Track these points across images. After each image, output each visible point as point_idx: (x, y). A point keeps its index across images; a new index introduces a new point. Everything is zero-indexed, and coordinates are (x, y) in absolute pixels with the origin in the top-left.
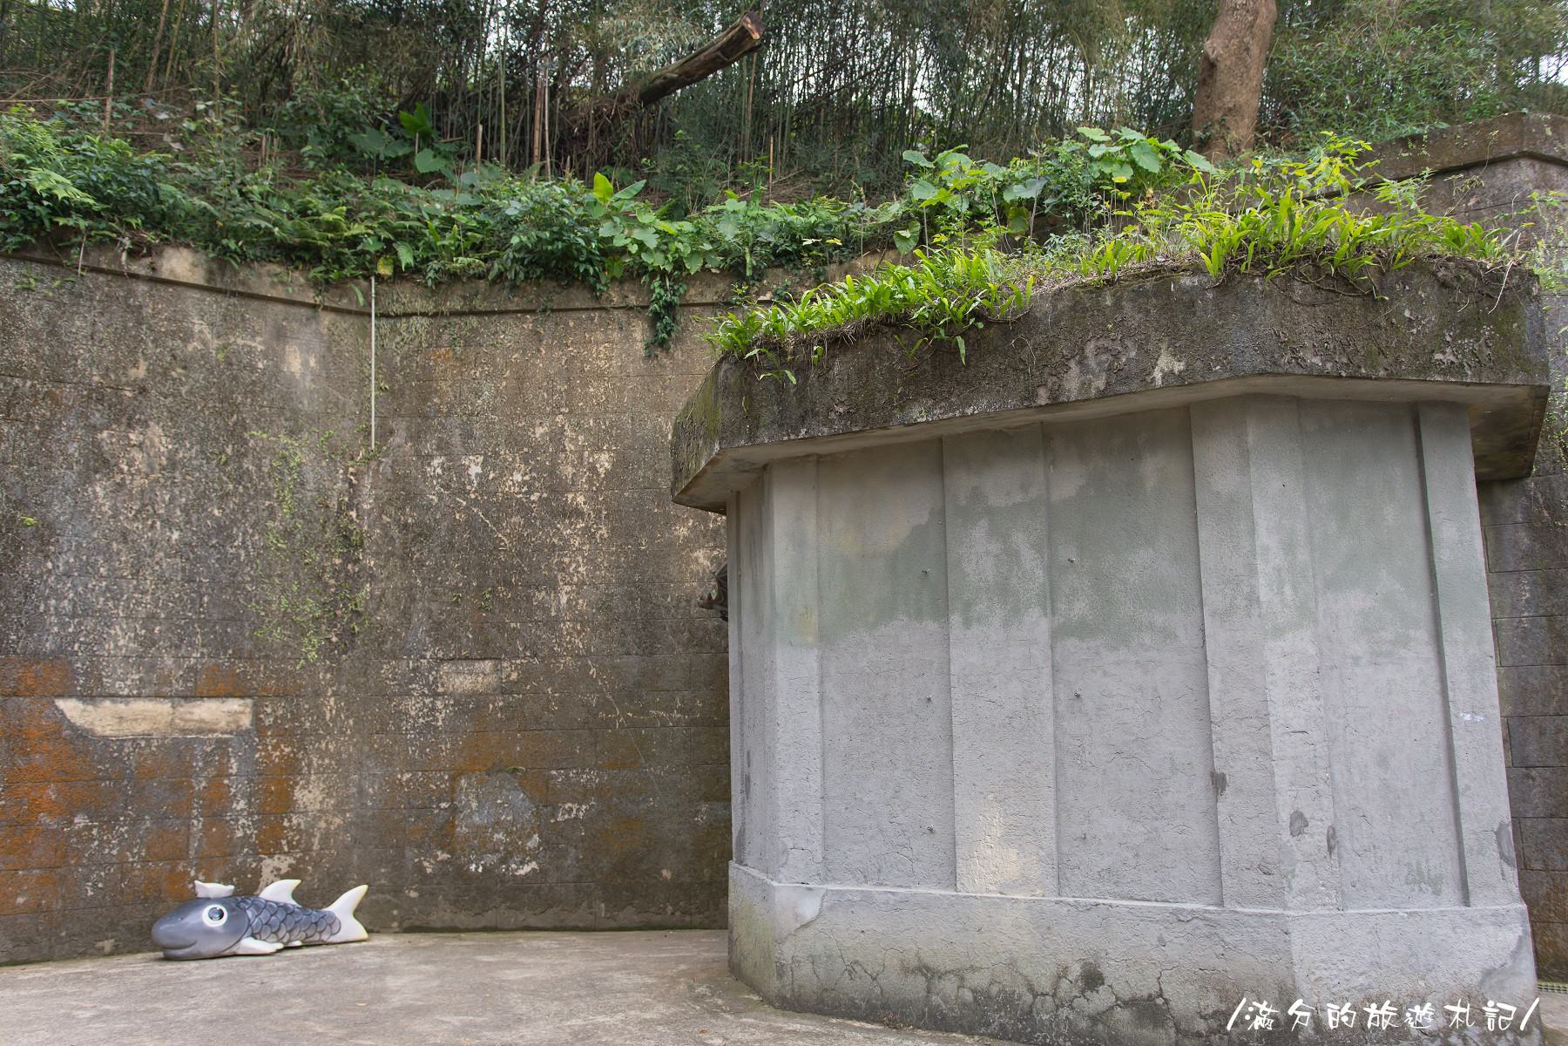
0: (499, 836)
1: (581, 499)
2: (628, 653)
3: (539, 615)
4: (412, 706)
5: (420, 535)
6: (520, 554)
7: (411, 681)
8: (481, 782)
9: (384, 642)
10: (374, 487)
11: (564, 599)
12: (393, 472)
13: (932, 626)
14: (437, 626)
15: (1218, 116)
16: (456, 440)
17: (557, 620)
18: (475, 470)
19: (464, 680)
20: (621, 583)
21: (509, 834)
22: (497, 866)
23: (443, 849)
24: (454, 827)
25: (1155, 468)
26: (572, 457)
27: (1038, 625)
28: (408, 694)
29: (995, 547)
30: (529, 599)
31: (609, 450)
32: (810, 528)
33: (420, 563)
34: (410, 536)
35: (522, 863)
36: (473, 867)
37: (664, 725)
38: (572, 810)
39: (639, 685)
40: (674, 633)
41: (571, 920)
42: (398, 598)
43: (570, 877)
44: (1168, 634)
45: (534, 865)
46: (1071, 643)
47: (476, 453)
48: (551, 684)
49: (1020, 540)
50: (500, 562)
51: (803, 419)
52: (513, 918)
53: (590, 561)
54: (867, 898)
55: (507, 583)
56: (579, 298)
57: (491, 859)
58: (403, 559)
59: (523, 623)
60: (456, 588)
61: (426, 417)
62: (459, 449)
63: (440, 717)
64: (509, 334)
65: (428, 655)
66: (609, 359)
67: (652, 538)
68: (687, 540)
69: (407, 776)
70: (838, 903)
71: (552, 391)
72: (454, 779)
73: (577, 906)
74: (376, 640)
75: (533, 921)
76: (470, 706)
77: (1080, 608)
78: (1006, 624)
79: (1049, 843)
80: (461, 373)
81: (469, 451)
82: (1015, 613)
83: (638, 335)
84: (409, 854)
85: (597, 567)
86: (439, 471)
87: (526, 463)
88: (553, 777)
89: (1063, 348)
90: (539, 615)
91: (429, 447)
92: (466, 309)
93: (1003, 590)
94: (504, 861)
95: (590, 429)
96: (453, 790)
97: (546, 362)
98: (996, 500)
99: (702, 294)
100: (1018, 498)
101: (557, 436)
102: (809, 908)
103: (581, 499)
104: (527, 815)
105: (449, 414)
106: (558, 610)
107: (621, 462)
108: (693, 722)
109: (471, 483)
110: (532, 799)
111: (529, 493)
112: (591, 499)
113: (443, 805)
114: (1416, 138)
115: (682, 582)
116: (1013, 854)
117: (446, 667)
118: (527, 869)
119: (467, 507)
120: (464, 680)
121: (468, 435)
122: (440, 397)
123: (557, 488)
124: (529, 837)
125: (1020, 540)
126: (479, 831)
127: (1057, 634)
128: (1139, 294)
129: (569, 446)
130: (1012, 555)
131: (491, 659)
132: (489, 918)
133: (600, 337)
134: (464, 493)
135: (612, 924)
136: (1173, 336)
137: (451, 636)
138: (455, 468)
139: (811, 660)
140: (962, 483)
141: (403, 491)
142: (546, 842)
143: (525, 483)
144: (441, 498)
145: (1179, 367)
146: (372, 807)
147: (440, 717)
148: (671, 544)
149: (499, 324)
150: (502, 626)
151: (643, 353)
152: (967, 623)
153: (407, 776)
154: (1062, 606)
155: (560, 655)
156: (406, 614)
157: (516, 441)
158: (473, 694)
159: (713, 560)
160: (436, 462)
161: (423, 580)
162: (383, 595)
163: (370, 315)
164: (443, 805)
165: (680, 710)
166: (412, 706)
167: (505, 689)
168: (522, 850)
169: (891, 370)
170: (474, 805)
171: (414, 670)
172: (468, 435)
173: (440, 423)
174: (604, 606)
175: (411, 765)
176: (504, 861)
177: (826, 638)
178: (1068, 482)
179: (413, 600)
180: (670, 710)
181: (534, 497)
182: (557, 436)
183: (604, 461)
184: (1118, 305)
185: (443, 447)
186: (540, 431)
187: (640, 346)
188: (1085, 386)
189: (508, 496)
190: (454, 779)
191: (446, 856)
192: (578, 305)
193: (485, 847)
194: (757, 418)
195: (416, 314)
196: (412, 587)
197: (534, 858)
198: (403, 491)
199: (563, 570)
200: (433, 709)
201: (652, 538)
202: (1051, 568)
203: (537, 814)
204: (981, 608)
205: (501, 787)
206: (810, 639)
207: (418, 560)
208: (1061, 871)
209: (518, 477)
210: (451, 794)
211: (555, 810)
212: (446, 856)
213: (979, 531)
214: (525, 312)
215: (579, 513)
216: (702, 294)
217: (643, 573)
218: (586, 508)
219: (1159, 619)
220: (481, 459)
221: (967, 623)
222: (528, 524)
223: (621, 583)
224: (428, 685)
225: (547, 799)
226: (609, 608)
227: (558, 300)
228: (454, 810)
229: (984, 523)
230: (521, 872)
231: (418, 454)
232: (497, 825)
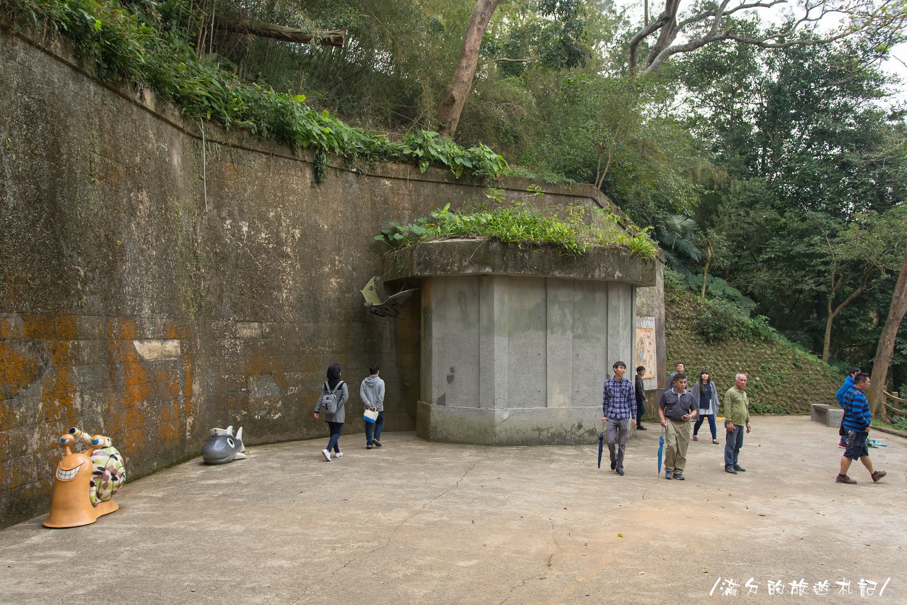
0: (266, 402)
1: (289, 250)
2: (309, 322)
3: (276, 303)
4: (226, 343)
5: (223, 258)
6: (266, 273)
7: (225, 331)
8: (258, 379)
9: (211, 311)
10: (201, 231)
11: (285, 296)
12: (209, 225)
13: (541, 333)
14: (234, 305)
15: (450, 120)
16: (236, 212)
17: (283, 305)
18: (245, 229)
19: (249, 331)
20: (306, 290)
21: (270, 401)
22: (266, 416)
23: (244, 410)
24: (248, 399)
25: (599, 296)
26: (285, 229)
27: (570, 335)
28: (224, 337)
29: (560, 312)
30: (271, 294)
31: (299, 228)
32: (506, 299)
33: (224, 273)
34: (219, 259)
35: (275, 414)
36: (256, 417)
37: (323, 353)
38: (293, 390)
39: (313, 335)
40: (325, 313)
41: (294, 436)
42: (216, 290)
43: (293, 419)
44: (599, 340)
45: (280, 414)
46: (577, 340)
47: (245, 220)
48: (282, 334)
49: (567, 311)
50: (258, 276)
51: (522, 268)
52: (273, 438)
53: (293, 279)
54: (523, 412)
55: (262, 286)
56: (287, 152)
57: (263, 413)
58: (216, 270)
59: (270, 306)
60: (240, 287)
61: (222, 198)
62: (237, 217)
63: (239, 348)
64: (256, 163)
65: (231, 318)
66: (297, 184)
67: (316, 271)
68: (328, 274)
69: (226, 376)
70: (512, 414)
71: (275, 195)
72: (247, 377)
73: (296, 430)
74: (208, 310)
75: (281, 438)
76: (249, 343)
77: (579, 331)
78: (562, 334)
79: (570, 393)
80: (238, 178)
81: (243, 219)
82: (564, 331)
83: (308, 175)
84: (230, 413)
85: (296, 282)
86: (229, 227)
87: (267, 229)
88: (286, 376)
89: (595, 264)
90: (276, 303)
91: (224, 214)
92: (239, 145)
93: (562, 325)
94: (269, 413)
95: (291, 217)
96: (247, 382)
97: (274, 181)
98: (561, 299)
99: (332, 162)
100: (567, 299)
101: (278, 218)
102: (506, 416)
103: (289, 250)
104: (277, 393)
105: (232, 198)
106: (283, 301)
107: (303, 235)
108: (333, 352)
109: (244, 235)
110: (278, 386)
111: (268, 244)
112: (293, 250)
113: (243, 390)
114: (569, 183)
115: (327, 292)
116: (562, 397)
117: (239, 325)
118: (277, 416)
119: (243, 247)
120: (249, 331)
121: (241, 211)
122: (229, 189)
123: (280, 243)
124: (278, 402)
125: (567, 311)
126: (258, 400)
127: (574, 337)
128: (613, 254)
129: (284, 224)
130: (565, 315)
131: (257, 322)
132: (264, 438)
133: (293, 173)
134: (241, 240)
135: (309, 436)
136: (620, 267)
137: (241, 310)
138: (236, 228)
139: (506, 340)
140: (552, 292)
141: (214, 236)
142: (283, 404)
143: (266, 239)
144: (231, 241)
145: (620, 275)
146: (212, 392)
147: (239, 348)
148: (323, 275)
149: (251, 156)
150: (261, 307)
151: (310, 185)
152: (552, 333)
153: (226, 376)
154: (575, 330)
155: (284, 322)
156: (220, 298)
157: (262, 217)
158: (251, 338)
159: (338, 283)
160: (228, 222)
161: (226, 281)
162: (209, 287)
163: (202, 139)
164: (243, 390)
165: (328, 347)
166: (226, 343)
167: (263, 336)
168: (275, 408)
169: (550, 258)
170: (256, 389)
171: (226, 326)
172: (241, 211)
173: (228, 202)
174: (299, 300)
175: (227, 371)
176: (269, 413)
177: (510, 335)
178: (578, 296)
179: (223, 291)
180: (324, 346)
181: (270, 246)
182: (278, 218)
183: (297, 233)
184: (608, 255)
185: (231, 215)
186: (272, 214)
187: (309, 181)
188: (600, 275)
189: (260, 244)
190: (247, 377)
191: (246, 413)
192: (285, 155)
193: (260, 409)
194: (507, 264)
195: (216, 142)
196: (221, 284)
197: (280, 411)
198: (214, 236)
199: (284, 282)
200: (236, 345)
201: (316, 271)
202: (574, 320)
203: (280, 392)
204: (556, 329)
205: (266, 381)
206: (506, 334)
207: (223, 271)
208: (572, 399)
209: (263, 235)
210: (246, 384)
211: (287, 390)
212: (246, 413)
213: (556, 307)
214: (263, 153)
215: (288, 256)
216: (332, 162)
217: (313, 287)
218: (291, 254)
219: (597, 336)
220: (247, 224)
221: (552, 333)
222: (269, 259)
223: (306, 290)
224: (232, 333)
225: (284, 387)
226: (302, 301)
227: (277, 151)
228: (248, 392)
229: (557, 305)
230: (275, 418)
231: (219, 216)
232: (266, 398)
